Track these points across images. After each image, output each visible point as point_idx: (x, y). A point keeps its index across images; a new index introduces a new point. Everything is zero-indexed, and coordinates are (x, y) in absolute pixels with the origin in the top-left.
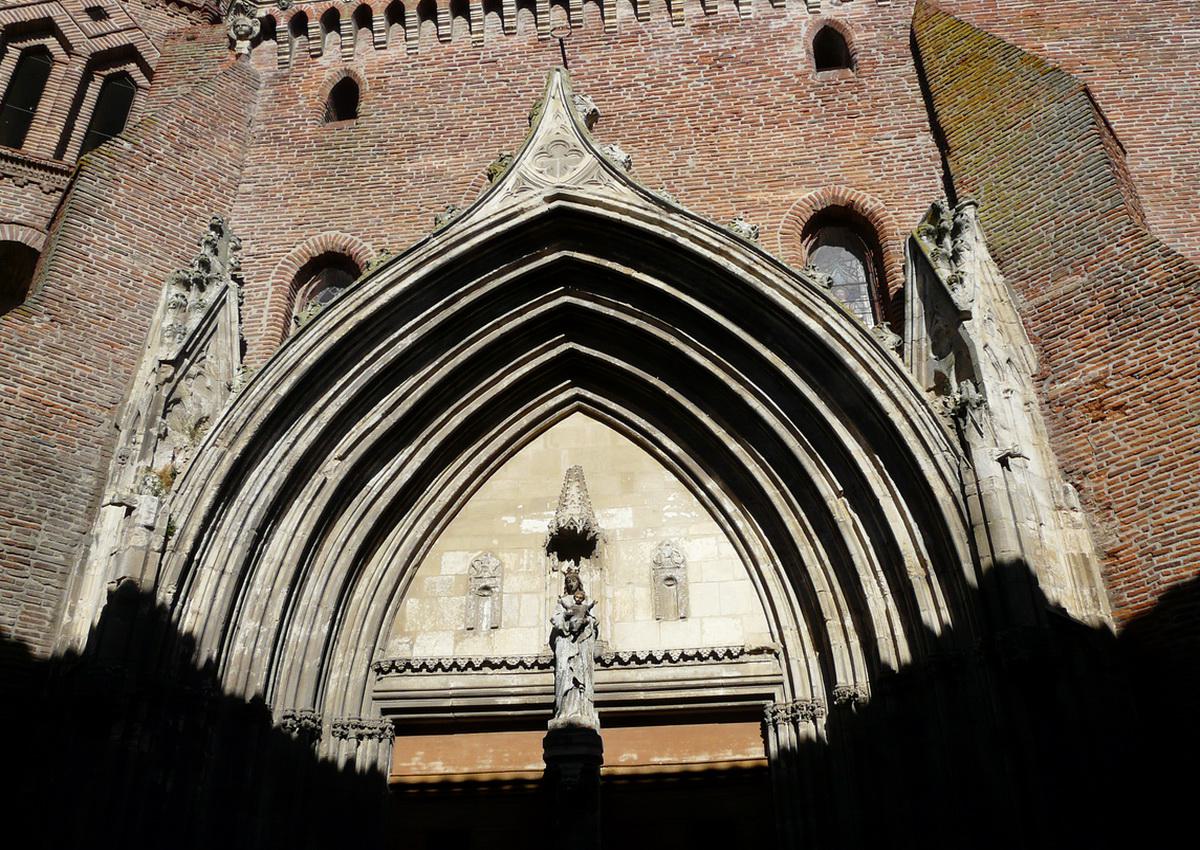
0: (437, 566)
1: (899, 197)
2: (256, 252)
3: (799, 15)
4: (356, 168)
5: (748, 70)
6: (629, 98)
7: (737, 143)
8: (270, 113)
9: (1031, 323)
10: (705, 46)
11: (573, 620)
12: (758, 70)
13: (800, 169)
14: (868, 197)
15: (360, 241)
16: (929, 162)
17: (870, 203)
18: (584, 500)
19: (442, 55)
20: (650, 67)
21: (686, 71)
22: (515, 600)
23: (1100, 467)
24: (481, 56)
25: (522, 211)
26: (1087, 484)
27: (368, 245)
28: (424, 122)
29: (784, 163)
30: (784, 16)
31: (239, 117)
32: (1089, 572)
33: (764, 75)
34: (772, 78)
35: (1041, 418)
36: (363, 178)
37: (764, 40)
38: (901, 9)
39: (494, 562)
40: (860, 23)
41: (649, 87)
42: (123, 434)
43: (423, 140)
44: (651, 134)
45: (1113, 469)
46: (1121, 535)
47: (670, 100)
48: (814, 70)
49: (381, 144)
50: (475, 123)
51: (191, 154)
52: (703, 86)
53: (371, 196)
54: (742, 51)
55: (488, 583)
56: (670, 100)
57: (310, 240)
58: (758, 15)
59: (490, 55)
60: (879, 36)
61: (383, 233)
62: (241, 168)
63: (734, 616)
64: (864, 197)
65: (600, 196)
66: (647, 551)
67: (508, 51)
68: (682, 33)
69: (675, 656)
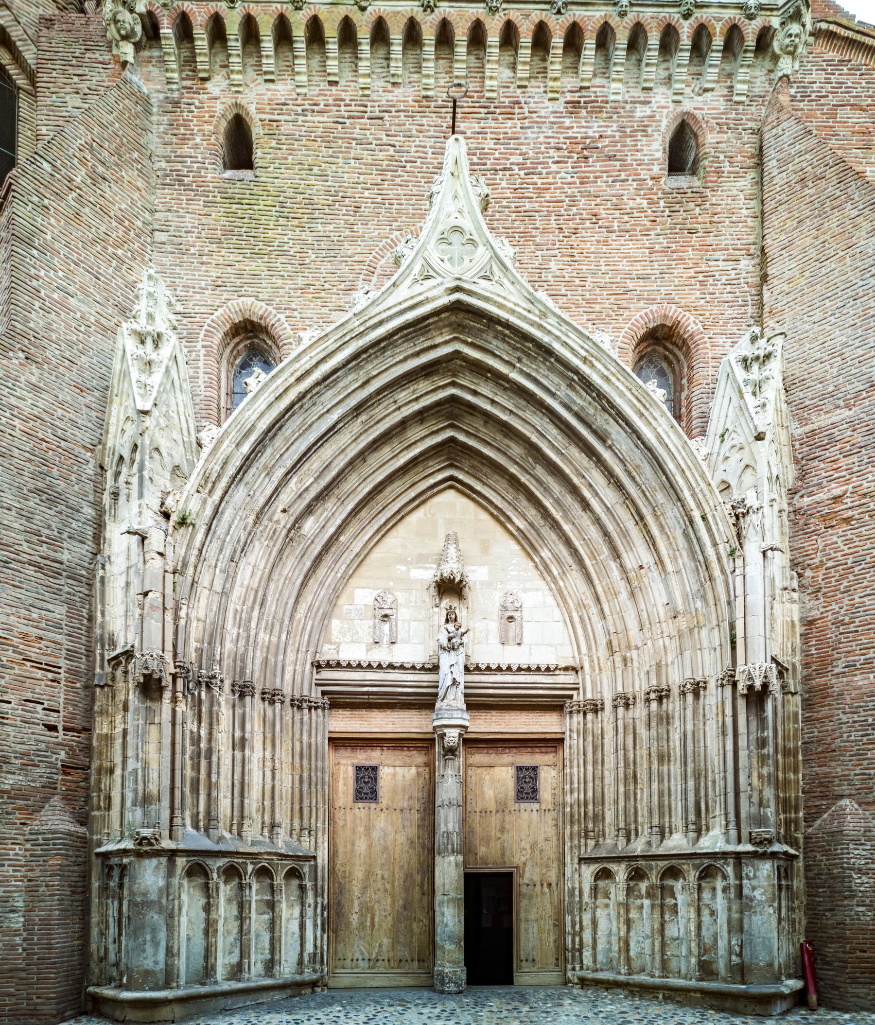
0: (352, 598)
1: (715, 323)
2: (182, 311)
3: (663, 103)
4: (261, 230)
5: (610, 166)
6: (504, 184)
7: (593, 250)
8: (169, 148)
9: (797, 447)
10: (575, 130)
11: (454, 640)
12: (618, 168)
13: (642, 284)
14: (692, 318)
15: (274, 312)
16: (746, 289)
17: (692, 325)
18: (459, 558)
19: (331, 102)
20: (524, 148)
21: (556, 159)
22: (406, 625)
23: (821, 561)
24: (369, 109)
25: (427, 300)
26: (808, 573)
27: (282, 317)
28: (319, 185)
29: (628, 276)
30: (649, 102)
31: (140, 148)
32: (794, 632)
33: (623, 174)
34: (630, 178)
35: (787, 523)
36: (268, 243)
37: (628, 130)
38: (753, 108)
39: (390, 599)
40: (715, 121)
41: (522, 173)
42: (109, 475)
43: (320, 207)
44: (522, 230)
45: (830, 564)
46: (822, 610)
47: (541, 191)
48: (666, 173)
49: (282, 205)
50: (366, 193)
51: (104, 186)
52: (570, 180)
53: (278, 265)
54: (607, 141)
55: (388, 612)
56: (541, 191)
57: (229, 304)
58: (627, 98)
59: (377, 109)
60: (728, 141)
61: (293, 306)
62: (153, 212)
63: (551, 645)
64: (688, 319)
65: (492, 293)
66: (497, 598)
67: (393, 106)
68: (556, 109)
69: (515, 668)
